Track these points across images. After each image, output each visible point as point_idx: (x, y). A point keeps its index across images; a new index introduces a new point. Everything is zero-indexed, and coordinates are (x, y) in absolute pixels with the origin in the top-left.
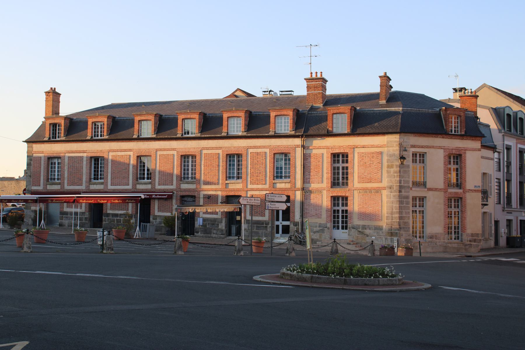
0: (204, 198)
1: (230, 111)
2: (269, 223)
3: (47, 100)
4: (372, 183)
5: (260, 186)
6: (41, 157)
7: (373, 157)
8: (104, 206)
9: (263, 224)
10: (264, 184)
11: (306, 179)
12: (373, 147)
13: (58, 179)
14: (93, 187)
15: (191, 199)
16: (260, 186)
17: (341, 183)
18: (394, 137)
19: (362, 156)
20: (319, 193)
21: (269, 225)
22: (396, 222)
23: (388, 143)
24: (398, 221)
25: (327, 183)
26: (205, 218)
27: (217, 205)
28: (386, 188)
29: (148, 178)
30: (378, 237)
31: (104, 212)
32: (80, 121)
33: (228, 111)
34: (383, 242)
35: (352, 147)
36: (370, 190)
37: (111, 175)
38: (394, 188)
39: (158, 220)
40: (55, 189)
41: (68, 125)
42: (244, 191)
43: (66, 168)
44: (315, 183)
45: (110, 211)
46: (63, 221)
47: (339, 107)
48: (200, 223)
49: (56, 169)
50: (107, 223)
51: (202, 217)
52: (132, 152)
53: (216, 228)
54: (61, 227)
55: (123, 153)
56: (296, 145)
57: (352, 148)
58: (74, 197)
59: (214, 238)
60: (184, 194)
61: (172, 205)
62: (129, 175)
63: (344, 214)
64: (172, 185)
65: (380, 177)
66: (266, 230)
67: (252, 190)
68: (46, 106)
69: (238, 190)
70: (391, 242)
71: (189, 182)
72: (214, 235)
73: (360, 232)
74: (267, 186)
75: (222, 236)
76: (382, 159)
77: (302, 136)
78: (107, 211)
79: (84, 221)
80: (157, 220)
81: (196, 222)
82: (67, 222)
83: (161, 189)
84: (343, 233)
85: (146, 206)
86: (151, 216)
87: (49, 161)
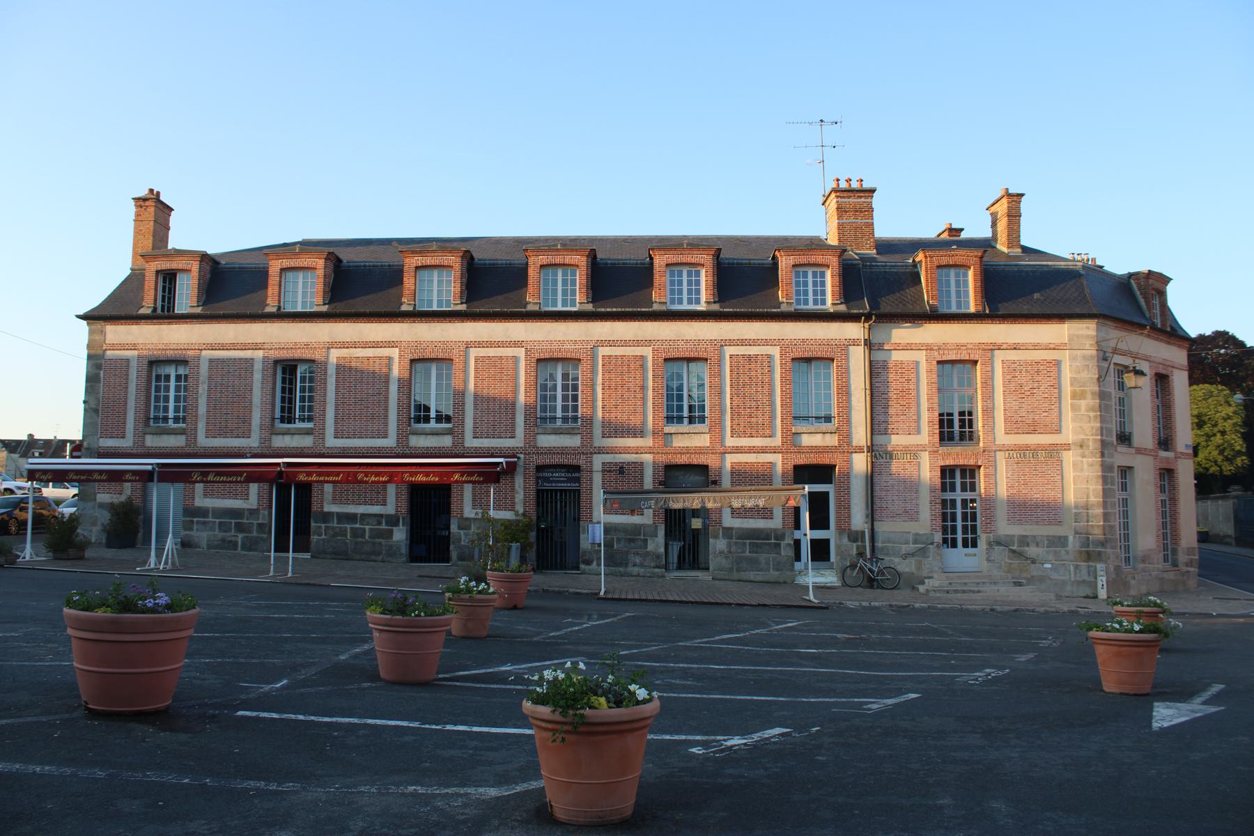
0: (603, 471)
1: (675, 249)
3: (140, 218)
4: (1039, 433)
5: (757, 442)
6: (128, 361)
7: (1038, 372)
8: (315, 493)
9: (768, 537)
10: (770, 437)
11: (877, 425)
12: (1037, 348)
13: (176, 420)
14: (279, 442)
15: (563, 475)
16: (757, 442)
18: (1085, 325)
19: (1010, 368)
20: (912, 458)
21: (784, 541)
22: (1098, 526)
23: (1070, 339)
24: (1102, 523)
25: (931, 434)
27: (768, 487)
28: (1072, 447)
30: (1060, 565)
31: (314, 508)
32: (239, 268)
33: (671, 249)
34: (1070, 575)
35: (989, 347)
36: (1035, 450)
37: (337, 409)
38: (1088, 446)
41: (208, 276)
42: (716, 453)
43: (203, 389)
45: (333, 506)
46: (194, 533)
47: (954, 250)
49: (172, 394)
50: (323, 539)
52: (397, 350)
53: (641, 551)
54: (188, 550)
55: (369, 352)
57: (989, 350)
58: (278, 464)
59: (636, 576)
60: (547, 460)
61: (513, 489)
62: (386, 409)
63: (949, 511)
64: (514, 437)
65: (1056, 421)
66: (777, 554)
67: (738, 450)
68: (135, 232)
69: (700, 451)
71: (561, 431)
72: (636, 570)
73: (1014, 552)
74: (777, 441)
75: (656, 570)
76: (1059, 377)
77: (868, 317)
78: (322, 507)
79: (255, 534)
81: (582, 536)
82: (205, 536)
83: (480, 448)
84: (966, 555)
86: (452, 521)
87: (152, 370)
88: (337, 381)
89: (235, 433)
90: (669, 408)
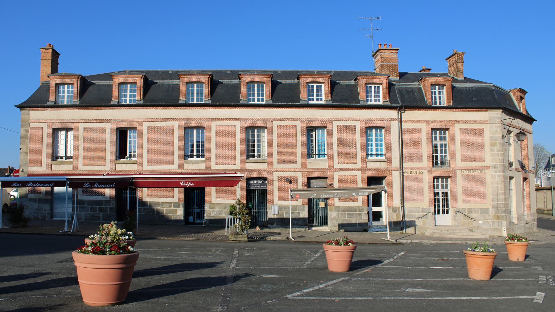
2: (363, 209)
9: (356, 211)
15: (258, 182)
17: (439, 162)
19: (464, 132)
21: (363, 212)
22: (502, 204)
25: (429, 162)
26: (281, 206)
29: (198, 156)
34: (490, 226)
37: (148, 151)
38: (498, 168)
39: (217, 209)
40: (64, 170)
44: (416, 162)
48: (274, 212)
50: (143, 215)
51: (276, 205)
56: (391, 118)
69: (381, 169)
70: (499, 226)
80: (215, 209)
82: (84, 214)
83: (219, 170)
85: (195, 191)
88: (148, 138)
89: (346, 161)
90: (248, 151)
